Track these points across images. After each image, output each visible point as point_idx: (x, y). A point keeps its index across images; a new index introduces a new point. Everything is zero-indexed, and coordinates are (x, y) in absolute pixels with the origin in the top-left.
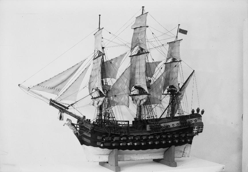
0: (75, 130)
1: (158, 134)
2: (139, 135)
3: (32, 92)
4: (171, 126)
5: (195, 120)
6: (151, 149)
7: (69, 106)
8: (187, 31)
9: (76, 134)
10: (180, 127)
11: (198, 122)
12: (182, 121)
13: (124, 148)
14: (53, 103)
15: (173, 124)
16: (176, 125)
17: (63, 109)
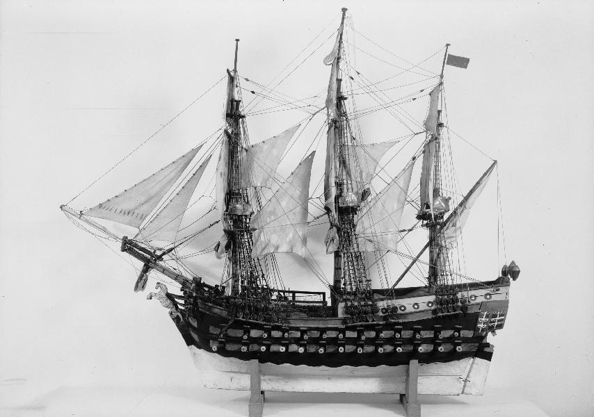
0: (174, 310)
1: (371, 328)
2: (317, 329)
3: (87, 221)
4: (410, 309)
5: (486, 295)
6: (309, 365)
7: (164, 254)
8: (467, 60)
9: (177, 320)
10: (434, 312)
11: (494, 301)
12: (444, 295)
13: (278, 359)
14: (129, 246)
15: (416, 304)
16: (423, 307)
17: (150, 261)
